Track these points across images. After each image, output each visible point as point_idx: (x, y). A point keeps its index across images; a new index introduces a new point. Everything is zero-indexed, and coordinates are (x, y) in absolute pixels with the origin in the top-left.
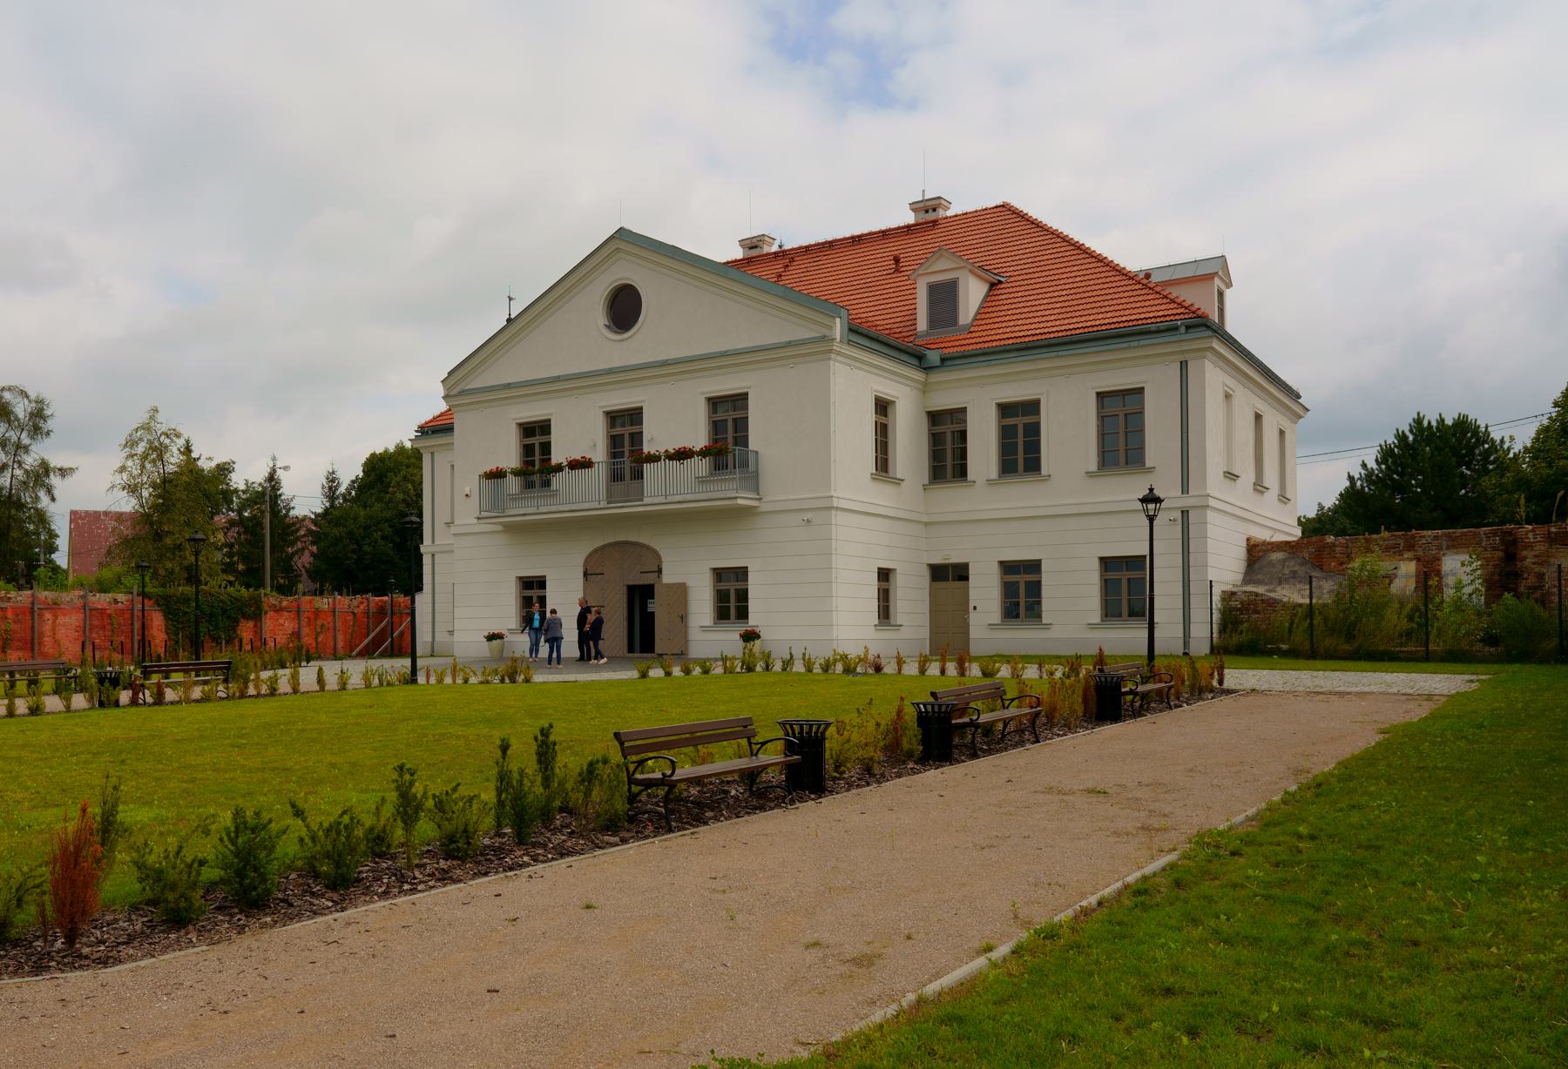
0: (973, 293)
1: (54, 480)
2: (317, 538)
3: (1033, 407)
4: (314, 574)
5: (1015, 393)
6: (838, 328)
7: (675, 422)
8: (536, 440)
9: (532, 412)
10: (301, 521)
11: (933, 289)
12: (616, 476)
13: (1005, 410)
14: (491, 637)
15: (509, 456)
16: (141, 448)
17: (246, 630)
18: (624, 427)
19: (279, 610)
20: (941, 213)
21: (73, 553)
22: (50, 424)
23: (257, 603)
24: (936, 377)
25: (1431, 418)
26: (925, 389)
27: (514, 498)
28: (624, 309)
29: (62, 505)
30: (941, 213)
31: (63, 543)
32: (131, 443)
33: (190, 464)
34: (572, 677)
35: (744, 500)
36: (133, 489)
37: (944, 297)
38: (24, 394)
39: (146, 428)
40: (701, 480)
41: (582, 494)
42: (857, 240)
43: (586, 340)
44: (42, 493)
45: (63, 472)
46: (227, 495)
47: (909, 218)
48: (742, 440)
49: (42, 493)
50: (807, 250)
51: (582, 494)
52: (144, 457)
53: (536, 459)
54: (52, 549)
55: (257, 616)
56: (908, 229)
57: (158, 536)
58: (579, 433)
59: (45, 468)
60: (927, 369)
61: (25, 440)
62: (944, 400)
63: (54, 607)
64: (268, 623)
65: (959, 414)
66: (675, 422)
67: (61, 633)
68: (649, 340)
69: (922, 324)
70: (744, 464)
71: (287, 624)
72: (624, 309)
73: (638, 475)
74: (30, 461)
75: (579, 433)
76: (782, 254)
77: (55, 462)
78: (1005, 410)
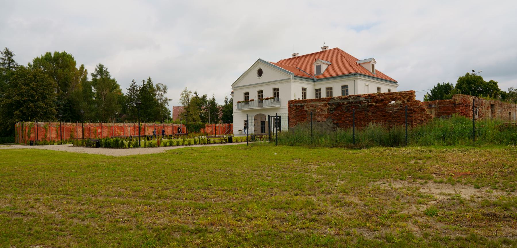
0: (324, 68)
1: (168, 101)
2: (223, 111)
3: (331, 88)
4: (222, 119)
5: (329, 86)
6: (292, 77)
7: (268, 93)
8: (247, 96)
9: (246, 91)
10: (219, 107)
11: (317, 66)
12: (259, 102)
13: (327, 89)
14: (239, 131)
15: (242, 99)
16: (184, 95)
17: (202, 130)
18: (260, 93)
19: (208, 126)
20: (327, 49)
21: (173, 116)
22: (167, 91)
23: (204, 125)
24: (316, 83)
25: (461, 76)
26: (314, 85)
27: (243, 106)
28: (260, 73)
29: (170, 107)
30: (327, 49)
31: (171, 113)
32: (182, 94)
33: (197, 97)
34: (5, 148)
35: (277, 106)
36: (183, 103)
37: (319, 68)
38: (162, 85)
39: (185, 91)
40: (272, 103)
41: (254, 105)
42: (311, 54)
43: (254, 78)
44: (166, 104)
45: (170, 100)
46: (206, 102)
47: (321, 50)
48: (278, 96)
49: (166, 104)
50: (303, 56)
51: (254, 105)
52: (185, 97)
53: (247, 100)
54: (169, 114)
55: (204, 128)
56: (320, 53)
57: (188, 112)
58: (253, 96)
59: (167, 99)
60: (314, 82)
61: (163, 94)
62: (318, 87)
63: (167, 126)
64: (206, 129)
65: (320, 90)
66: (268, 93)
67: (168, 131)
68: (265, 78)
69: (315, 73)
70: (278, 100)
71: (210, 129)
72: (260, 73)
73: (262, 102)
74: (164, 98)
75: (253, 96)
76: (299, 57)
77: (168, 98)
78: (327, 89)
